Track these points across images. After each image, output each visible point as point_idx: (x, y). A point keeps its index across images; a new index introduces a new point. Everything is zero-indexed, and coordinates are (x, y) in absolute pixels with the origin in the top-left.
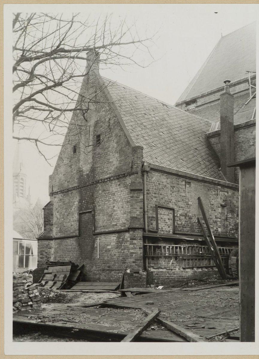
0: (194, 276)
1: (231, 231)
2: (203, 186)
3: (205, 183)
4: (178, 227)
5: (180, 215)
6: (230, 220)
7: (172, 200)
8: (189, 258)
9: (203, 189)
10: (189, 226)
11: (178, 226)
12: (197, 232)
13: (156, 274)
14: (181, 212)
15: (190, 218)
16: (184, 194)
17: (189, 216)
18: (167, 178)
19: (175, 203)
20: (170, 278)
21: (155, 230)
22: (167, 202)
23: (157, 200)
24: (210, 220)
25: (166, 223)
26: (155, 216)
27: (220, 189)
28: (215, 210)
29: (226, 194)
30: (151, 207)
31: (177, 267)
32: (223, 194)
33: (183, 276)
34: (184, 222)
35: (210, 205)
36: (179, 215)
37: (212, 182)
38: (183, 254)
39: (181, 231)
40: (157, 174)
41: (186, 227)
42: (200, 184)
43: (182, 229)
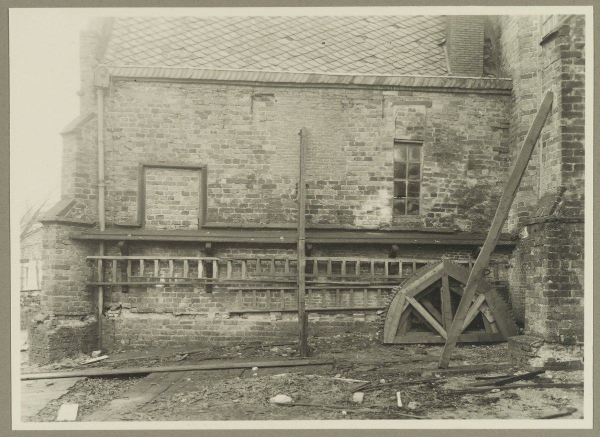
0: (259, 334)
1: (435, 213)
2: (323, 97)
3: (330, 90)
4: (222, 210)
5: (229, 181)
6: (435, 181)
7: (199, 146)
8: (237, 288)
9: (320, 105)
10: (263, 206)
11: (219, 208)
12: (291, 221)
13: (124, 327)
14: (232, 172)
15: (269, 186)
16: (246, 128)
17: (261, 181)
18: (186, 94)
19: (208, 152)
20: (172, 336)
21: (135, 221)
22: (183, 153)
23: (145, 150)
24: (346, 186)
25: (175, 203)
26: (136, 189)
27: (394, 98)
28: (370, 159)
29: (421, 109)
30: (126, 168)
31: (211, 309)
32: (406, 112)
33: (217, 334)
34: (242, 199)
35: (351, 144)
36: (224, 181)
37: (351, 84)
38: (200, 276)
39: (230, 220)
40: (147, 89)
41: (249, 211)
42: (312, 94)
43: (235, 216)
